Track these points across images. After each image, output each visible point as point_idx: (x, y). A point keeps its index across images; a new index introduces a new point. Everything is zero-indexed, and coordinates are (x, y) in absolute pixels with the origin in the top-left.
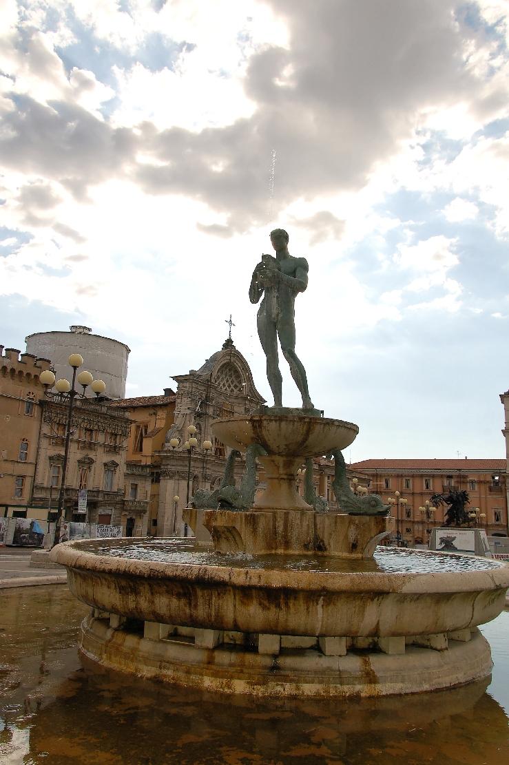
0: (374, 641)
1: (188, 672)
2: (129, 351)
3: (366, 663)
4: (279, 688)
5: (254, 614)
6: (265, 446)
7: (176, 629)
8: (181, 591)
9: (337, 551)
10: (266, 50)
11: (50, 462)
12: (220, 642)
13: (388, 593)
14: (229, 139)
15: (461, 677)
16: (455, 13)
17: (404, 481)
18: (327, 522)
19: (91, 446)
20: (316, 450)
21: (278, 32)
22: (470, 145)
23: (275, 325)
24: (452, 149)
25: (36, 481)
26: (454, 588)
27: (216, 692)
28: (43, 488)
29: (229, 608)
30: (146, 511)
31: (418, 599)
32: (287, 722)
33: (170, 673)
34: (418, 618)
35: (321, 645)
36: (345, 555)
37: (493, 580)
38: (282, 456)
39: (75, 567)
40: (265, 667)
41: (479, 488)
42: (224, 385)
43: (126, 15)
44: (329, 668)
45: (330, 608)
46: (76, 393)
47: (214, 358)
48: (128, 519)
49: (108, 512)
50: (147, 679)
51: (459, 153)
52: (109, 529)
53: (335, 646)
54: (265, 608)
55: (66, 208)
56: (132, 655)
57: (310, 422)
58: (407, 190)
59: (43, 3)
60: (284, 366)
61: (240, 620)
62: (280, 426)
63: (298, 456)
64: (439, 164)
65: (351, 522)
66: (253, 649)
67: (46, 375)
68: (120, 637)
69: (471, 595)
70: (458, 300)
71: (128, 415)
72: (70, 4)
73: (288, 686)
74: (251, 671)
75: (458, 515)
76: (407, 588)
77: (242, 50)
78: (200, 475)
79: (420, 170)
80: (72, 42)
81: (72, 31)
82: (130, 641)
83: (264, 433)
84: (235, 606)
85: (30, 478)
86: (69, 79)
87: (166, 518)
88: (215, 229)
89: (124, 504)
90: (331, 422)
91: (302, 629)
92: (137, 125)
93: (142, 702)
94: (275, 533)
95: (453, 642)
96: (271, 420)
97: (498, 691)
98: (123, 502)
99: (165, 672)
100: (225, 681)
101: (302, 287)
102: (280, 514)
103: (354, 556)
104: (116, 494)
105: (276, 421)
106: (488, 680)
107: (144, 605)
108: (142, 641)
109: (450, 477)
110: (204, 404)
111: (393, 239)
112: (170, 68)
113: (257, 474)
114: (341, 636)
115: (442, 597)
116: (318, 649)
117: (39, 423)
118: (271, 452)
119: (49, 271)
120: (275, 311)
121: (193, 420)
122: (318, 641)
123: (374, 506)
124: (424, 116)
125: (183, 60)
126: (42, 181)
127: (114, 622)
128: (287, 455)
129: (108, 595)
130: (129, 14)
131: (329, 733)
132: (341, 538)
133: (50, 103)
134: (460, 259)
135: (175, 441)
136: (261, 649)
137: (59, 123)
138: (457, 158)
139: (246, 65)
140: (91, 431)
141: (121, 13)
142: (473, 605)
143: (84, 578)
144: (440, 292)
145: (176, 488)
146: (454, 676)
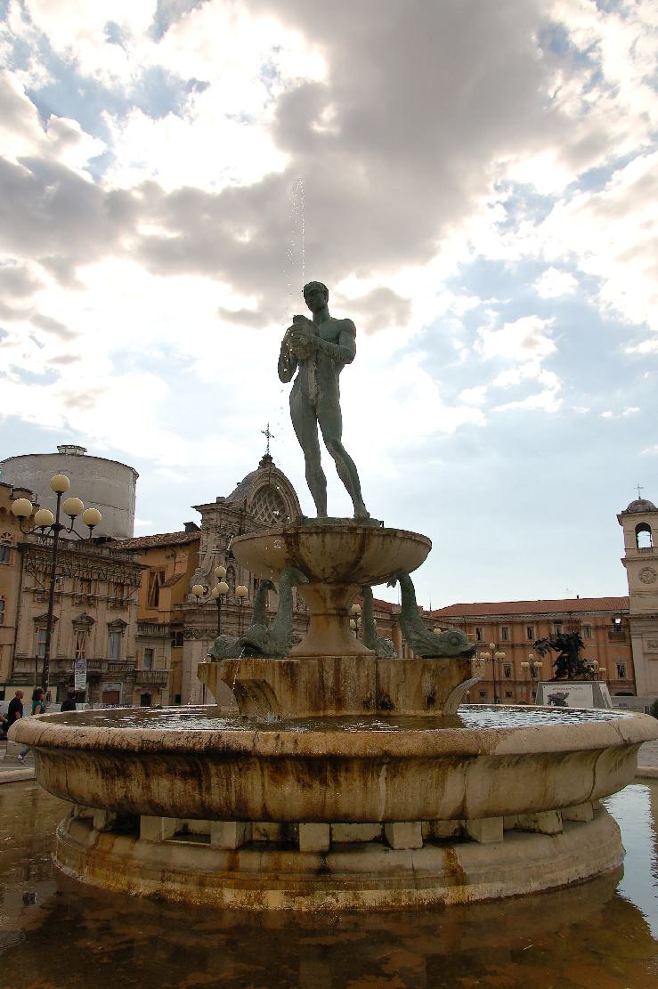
0: (460, 825)
1: (202, 884)
3: (450, 857)
4: (329, 899)
5: (291, 795)
6: (306, 570)
7: (185, 826)
8: (188, 768)
9: (406, 706)
10: (299, 85)
12: (248, 838)
13: (476, 756)
14: (256, 200)
15: (582, 870)
16: (537, 37)
17: (501, 630)
18: (393, 670)
19: (90, 601)
20: (374, 573)
21: (309, 60)
22: (563, 201)
23: (314, 408)
24: (541, 206)
25: (17, 651)
26: (567, 745)
28: (28, 659)
29: (256, 788)
31: (517, 762)
32: (348, 950)
33: (177, 886)
34: (518, 789)
35: (388, 837)
37: (620, 733)
38: (329, 583)
39: (39, 744)
40: (309, 870)
41: (597, 637)
43: (117, 48)
44: (400, 868)
45: (396, 780)
46: (62, 527)
47: (248, 480)
49: (115, 687)
53: (406, 835)
55: (49, 296)
56: (124, 866)
57: (364, 534)
58: (488, 258)
59: (8, 33)
60: (328, 464)
61: (273, 806)
63: (350, 583)
64: (526, 226)
65: (425, 668)
67: (22, 505)
68: (107, 841)
69: (591, 754)
70: (557, 397)
71: (137, 558)
72: (44, 35)
73: (342, 895)
74: (291, 878)
75: (570, 666)
76: (503, 747)
77: (268, 88)
79: (501, 235)
80: (48, 83)
81: (47, 68)
82: (121, 845)
83: (303, 551)
84: (263, 785)
85: (9, 647)
86: (46, 131)
88: (243, 317)
90: (393, 533)
91: (358, 812)
92: (136, 185)
93: (139, 932)
94: (323, 687)
95: (570, 823)
96: (311, 534)
97: (638, 886)
99: (169, 886)
100: (253, 893)
101: (349, 356)
102: (329, 660)
103: (431, 713)
104: (125, 663)
105: (317, 533)
106: (619, 873)
107: (136, 791)
108: (137, 845)
109: (558, 622)
111: (473, 322)
112: (176, 113)
114: (413, 820)
115: (552, 759)
116: (383, 842)
117: (19, 574)
118: (313, 579)
119: (28, 378)
120: (312, 390)
121: (224, 561)
122: (383, 830)
123: (455, 645)
124: (504, 165)
125: (193, 102)
126: (15, 262)
127: (99, 822)
128: (337, 582)
129: (87, 781)
130: (121, 45)
131: (406, 959)
132: (414, 689)
133: (21, 160)
134: (557, 345)
135: (198, 588)
136: (303, 846)
137: (35, 186)
138: (547, 218)
139: (273, 108)
140: (122, 585)
141: (110, 45)
142: (594, 770)
143: (54, 760)
144: (533, 387)
146: (573, 870)
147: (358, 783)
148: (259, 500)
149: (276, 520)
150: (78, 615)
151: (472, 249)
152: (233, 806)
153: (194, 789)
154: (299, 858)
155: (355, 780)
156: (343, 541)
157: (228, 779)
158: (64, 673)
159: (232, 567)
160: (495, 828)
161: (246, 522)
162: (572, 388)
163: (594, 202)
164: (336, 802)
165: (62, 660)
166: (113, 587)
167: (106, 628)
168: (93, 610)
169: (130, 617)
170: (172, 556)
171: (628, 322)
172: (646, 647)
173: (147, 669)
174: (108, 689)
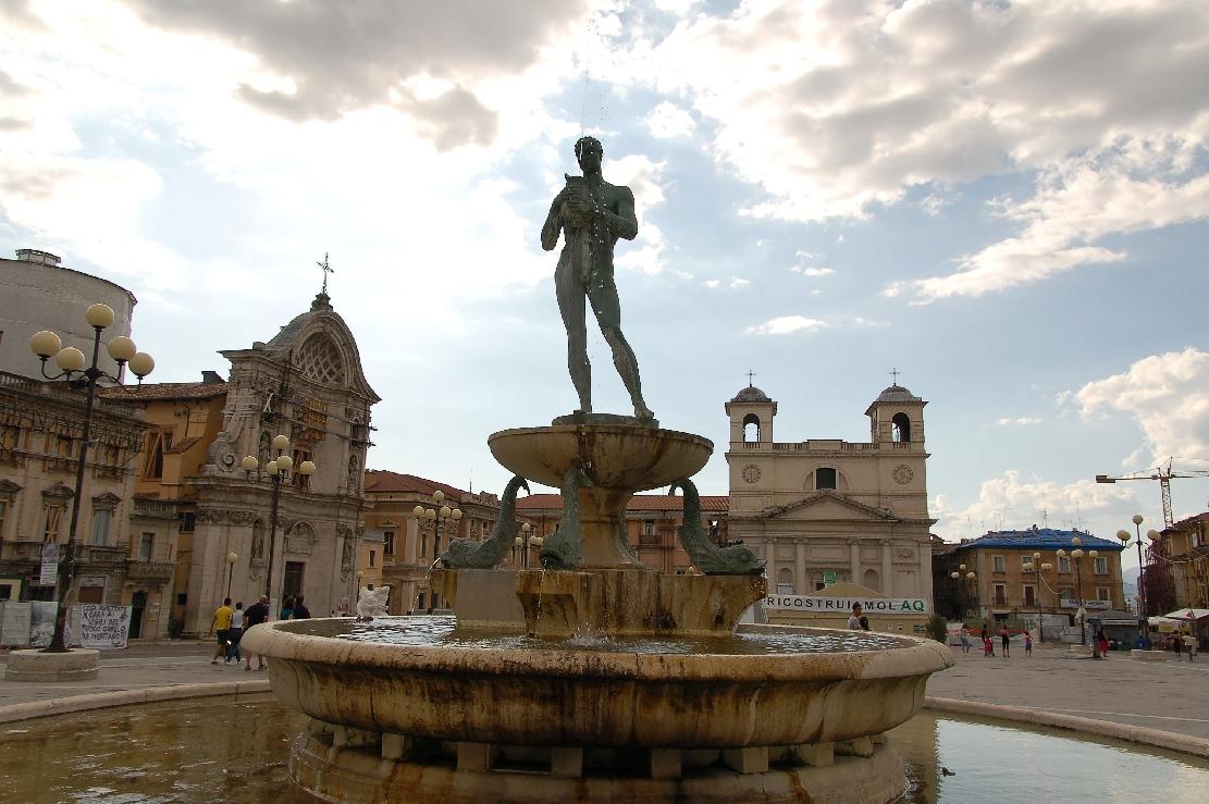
2: (133, 301)
8: (549, 692)
11: (44, 501)
30: (169, 579)
36: (708, 632)
42: (310, 369)
45: (766, 704)
47: (296, 324)
48: (135, 594)
49: (98, 582)
51: (672, 31)
52: (106, 612)
53: (755, 760)
54: (679, 710)
62: (622, 442)
66: (644, 772)
68: (410, 773)
70: (660, 256)
71: (139, 414)
79: (613, 51)
84: (634, 710)
87: (203, 591)
88: (273, 102)
89: (127, 568)
94: (605, 604)
96: (609, 433)
98: (127, 565)
102: (612, 573)
103: (718, 634)
104: (114, 551)
108: (457, 775)
109: (651, 521)
110: (279, 401)
113: (362, 515)
120: (586, 265)
121: (258, 426)
123: (745, 562)
128: (614, 488)
134: (666, 194)
138: (666, 39)
140: (69, 439)
145: (224, 540)
147: (730, 707)
148: (308, 350)
149: (328, 377)
150: (53, 484)
151: (576, 61)
152: (599, 731)
153: (554, 713)
155: (727, 704)
158: (26, 561)
159: (268, 434)
160: (824, 753)
163: (720, 30)
164: (708, 726)
167: (91, 502)
169: (125, 490)
170: (184, 413)
171: (744, 180)
173: (144, 559)
174: (89, 584)
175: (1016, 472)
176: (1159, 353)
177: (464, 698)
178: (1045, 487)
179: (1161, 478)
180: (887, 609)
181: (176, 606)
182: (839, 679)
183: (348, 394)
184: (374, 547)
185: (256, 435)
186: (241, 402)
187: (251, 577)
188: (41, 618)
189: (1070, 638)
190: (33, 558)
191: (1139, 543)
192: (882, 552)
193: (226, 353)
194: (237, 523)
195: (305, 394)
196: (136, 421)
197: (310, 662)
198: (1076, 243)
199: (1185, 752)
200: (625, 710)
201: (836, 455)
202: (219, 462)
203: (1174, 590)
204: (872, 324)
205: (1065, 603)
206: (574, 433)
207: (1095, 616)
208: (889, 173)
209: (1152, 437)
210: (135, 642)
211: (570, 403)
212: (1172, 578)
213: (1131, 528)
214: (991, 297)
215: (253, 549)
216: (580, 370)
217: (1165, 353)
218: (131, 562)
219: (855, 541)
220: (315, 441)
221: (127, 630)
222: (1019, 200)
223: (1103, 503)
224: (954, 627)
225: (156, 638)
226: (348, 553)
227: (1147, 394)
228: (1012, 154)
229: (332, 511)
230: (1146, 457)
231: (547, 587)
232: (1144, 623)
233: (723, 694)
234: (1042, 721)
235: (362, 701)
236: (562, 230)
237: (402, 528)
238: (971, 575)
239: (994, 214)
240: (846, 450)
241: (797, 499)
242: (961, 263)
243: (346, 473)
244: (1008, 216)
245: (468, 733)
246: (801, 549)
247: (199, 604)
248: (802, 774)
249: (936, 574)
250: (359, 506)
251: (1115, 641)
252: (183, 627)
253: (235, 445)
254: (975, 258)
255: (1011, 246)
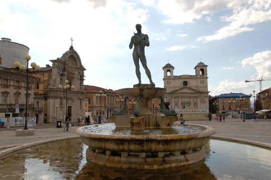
1: (140, 165)
2: (29, 49)
3: (185, 157)
4: (166, 166)
7: (129, 153)
8: (139, 143)
9: (163, 126)
11: (2, 94)
19: (19, 87)
27: (149, 169)
33: (134, 166)
42: (70, 63)
45: (180, 144)
50: (126, 168)
52: (31, 119)
54: (164, 145)
66: (157, 156)
68: (112, 158)
71: (33, 75)
73: (168, 165)
78: (63, 97)
84: (155, 146)
89: (34, 109)
94: (146, 122)
96: (146, 89)
99: (132, 166)
100: (151, 166)
105: (147, 89)
110: (64, 70)
113: (83, 95)
121: (59, 76)
140: (19, 82)
152: (149, 150)
153: (140, 147)
154: (159, 158)
156: (153, 91)
157: (148, 145)
158: (12, 108)
160: (191, 151)
161: (66, 66)
162: (150, 31)
165: (11, 105)
166: (15, 82)
168: (20, 90)
170: (43, 74)
172: (167, 100)
175: (227, 80)
176: (261, 52)
177: (122, 144)
178: (234, 83)
179: (260, 81)
180: (199, 112)
181: (45, 116)
182: (194, 138)
183: (79, 69)
184: (86, 102)
185: (59, 79)
186: (55, 72)
187: (60, 110)
188: (17, 121)
189: (238, 117)
190: (14, 108)
191: (254, 96)
192: (191, 99)
193: (51, 61)
194: (57, 98)
195: (69, 69)
196: (32, 77)
197: (92, 138)
198: (242, 26)
199: (261, 146)
200: (154, 146)
201: (187, 78)
202: (51, 85)
203: (261, 105)
204: (195, 47)
205: (238, 109)
206: (139, 89)
207: (244, 112)
208: (199, 11)
209: (258, 71)
210: (37, 124)
211: (137, 82)
212: (261, 103)
213: (252, 93)
214: (222, 40)
215: (60, 104)
216: (138, 74)
217: (262, 52)
218: (34, 108)
219: (192, 97)
220: (72, 79)
221: (36, 122)
222: (229, 17)
223: (247, 86)
224: (214, 115)
225: (41, 124)
226: (81, 104)
227: (257, 61)
228: (227, 6)
229: (77, 95)
230: (257, 76)
231: (135, 121)
232: (255, 113)
233: (172, 142)
234: (233, 140)
235: (102, 145)
236: (133, 45)
237: (92, 98)
238: (217, 104)
239: (223, 20)
240: (191, 77)
241: (178, 88)
242: (215, 32)
243: (79, 86)
244: (226, 20)
245: (124, 151)
246: (192, 99)
247: (50, 116)
248: (186, 155)
249: (209, 104)
250: (83, 93)
251: (248, 117)
252: (46, 121)
253: (55, 81)
254: (219, 31)
255: (227, 28)
